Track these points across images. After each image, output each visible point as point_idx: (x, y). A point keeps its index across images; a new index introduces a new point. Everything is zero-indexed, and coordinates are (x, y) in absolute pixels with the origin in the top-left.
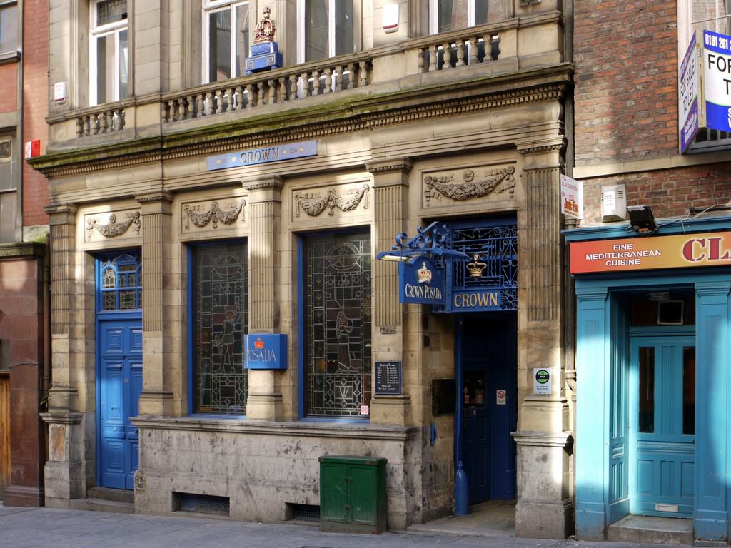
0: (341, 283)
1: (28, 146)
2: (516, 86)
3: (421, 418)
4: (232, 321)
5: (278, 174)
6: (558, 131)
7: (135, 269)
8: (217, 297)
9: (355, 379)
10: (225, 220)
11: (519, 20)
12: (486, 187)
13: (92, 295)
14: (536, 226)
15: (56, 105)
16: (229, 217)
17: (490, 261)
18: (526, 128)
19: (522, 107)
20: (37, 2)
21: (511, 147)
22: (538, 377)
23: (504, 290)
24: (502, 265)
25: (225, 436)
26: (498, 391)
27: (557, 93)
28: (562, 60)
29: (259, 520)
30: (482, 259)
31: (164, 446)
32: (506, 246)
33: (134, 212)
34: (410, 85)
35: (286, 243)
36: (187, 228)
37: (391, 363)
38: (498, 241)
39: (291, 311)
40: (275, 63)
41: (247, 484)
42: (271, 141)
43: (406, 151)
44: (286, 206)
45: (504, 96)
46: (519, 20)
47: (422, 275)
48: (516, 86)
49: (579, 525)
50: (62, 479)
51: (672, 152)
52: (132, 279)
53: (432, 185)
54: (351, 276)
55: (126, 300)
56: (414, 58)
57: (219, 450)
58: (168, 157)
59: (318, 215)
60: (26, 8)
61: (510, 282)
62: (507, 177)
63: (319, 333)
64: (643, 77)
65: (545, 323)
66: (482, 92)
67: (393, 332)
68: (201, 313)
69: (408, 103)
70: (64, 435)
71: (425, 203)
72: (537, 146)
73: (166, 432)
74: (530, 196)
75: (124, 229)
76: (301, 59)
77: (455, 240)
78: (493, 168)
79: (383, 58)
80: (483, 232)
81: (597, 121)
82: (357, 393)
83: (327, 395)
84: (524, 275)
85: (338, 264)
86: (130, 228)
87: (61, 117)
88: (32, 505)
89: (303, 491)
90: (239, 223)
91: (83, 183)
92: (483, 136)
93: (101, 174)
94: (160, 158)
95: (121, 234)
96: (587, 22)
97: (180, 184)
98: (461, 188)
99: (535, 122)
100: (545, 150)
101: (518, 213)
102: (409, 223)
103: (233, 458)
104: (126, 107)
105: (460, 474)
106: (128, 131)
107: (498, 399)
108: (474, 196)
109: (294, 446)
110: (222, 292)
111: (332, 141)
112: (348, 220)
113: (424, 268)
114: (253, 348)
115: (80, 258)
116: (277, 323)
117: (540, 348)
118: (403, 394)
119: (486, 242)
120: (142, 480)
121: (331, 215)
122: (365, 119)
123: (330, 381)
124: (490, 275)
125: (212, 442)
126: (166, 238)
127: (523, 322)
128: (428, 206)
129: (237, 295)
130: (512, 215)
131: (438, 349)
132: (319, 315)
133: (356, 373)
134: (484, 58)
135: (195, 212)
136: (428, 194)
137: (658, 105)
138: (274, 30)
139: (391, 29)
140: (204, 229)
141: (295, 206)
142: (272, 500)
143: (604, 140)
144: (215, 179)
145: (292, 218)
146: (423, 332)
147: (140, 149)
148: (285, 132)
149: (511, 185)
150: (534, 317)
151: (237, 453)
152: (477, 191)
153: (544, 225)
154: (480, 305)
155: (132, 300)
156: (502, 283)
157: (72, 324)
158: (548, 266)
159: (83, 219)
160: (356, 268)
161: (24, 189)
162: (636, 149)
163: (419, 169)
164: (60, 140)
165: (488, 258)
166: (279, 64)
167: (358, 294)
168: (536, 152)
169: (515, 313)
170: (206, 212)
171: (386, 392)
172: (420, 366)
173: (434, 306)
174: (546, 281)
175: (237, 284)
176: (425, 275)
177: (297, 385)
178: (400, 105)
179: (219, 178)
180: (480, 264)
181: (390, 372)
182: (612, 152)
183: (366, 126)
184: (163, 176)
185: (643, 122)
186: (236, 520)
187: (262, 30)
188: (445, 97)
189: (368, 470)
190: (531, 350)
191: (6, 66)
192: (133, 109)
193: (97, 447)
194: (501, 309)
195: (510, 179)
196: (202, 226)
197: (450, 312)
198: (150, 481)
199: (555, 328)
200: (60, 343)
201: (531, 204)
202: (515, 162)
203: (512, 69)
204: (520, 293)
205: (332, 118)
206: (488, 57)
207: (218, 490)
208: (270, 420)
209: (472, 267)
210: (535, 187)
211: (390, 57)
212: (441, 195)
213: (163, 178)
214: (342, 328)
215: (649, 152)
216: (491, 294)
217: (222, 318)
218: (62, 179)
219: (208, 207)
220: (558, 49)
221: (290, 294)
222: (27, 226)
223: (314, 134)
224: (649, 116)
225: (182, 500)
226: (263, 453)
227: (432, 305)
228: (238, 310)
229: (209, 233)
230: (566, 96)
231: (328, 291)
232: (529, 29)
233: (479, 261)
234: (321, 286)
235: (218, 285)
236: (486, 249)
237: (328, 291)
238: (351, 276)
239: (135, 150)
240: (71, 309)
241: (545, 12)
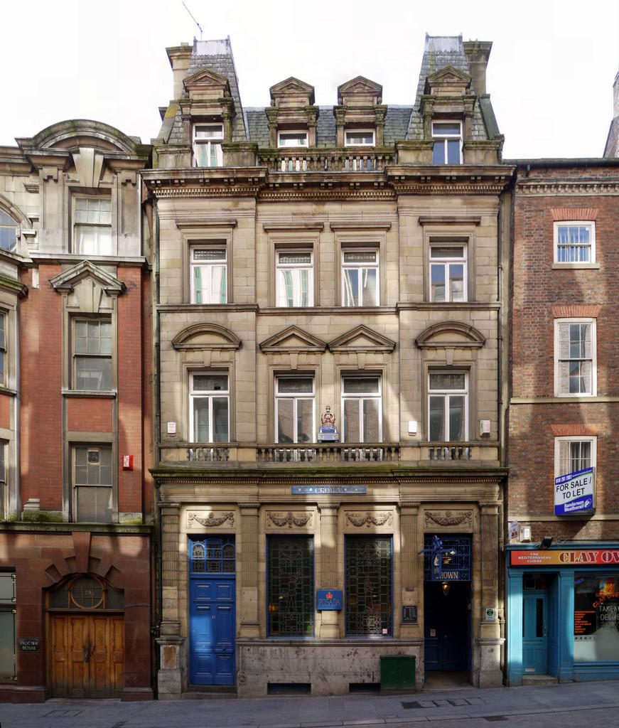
2: (483, 474)
18: (483, 494)
19: (481, 485)
22: (488, 612)
25: (306, 648)
28: (501, 466)
29: (331, 694)
31: (260, 656)
35: (341, 540)
41: (323, 675)
48: (483, 474)
49: (511, 679)
50: (175, 681)
51: (550, 514)
52: (218, 554)
57: (302, 657)
59: (360, 526)
64: (540, 480)
65: (491, 588)
66: (466, 474)
69: (426, 474)
70: (175, 652)
71: (425, 526)
73: (262, 648)
75: (221, 522)
79: (406, 449)
80: (450, 542)
81: (518, 496)
86: (225, 522)
88: (150, 699)
89: (361, 676)
90: (308, 526)
93: (207, 486)
96: (514, 450)
100: (493, 506)
103: (312, 661)
104: (231, 447)
109: (353, 652)
111: (376, 487)
112: (380, 530)
115: (183, 538)
120: (244, 677)
121: (368, 526)
125: (297, 652)
127: (477, 586)
130: (470, 536)
135: (276, 517)
137: (546, 493)
139: (412, 434)
140: (283, 527)
142: (342, 682)
143: (523, 505)
147: (246, 475)
151: (315, 658)
159: (186, 514)
160: (376, 556)
162: (536, 511)
164: (171, 460)
170: (283, 517)
171: (409, 621)
178: (421, 474)
179: (300, 499)
182: (525, 511)
185: (539, 499)
186: (316, 696)
188: (447, 474)
191: (103, 400)
193: (193, 660)
196: (280, 526)
198: (250, 678)
200: (169, 593)
205: (381, 475)
207: (302, 679)
208: (337, 638)
215: (541, 513)
217: (287, 580)
219: (285, 515)
222: (123, 512)
224: (542, 497)
225: (273, 688)
226: (333, 656)
229: (285, 530)
230: (503, 483)
239: (243, 475)
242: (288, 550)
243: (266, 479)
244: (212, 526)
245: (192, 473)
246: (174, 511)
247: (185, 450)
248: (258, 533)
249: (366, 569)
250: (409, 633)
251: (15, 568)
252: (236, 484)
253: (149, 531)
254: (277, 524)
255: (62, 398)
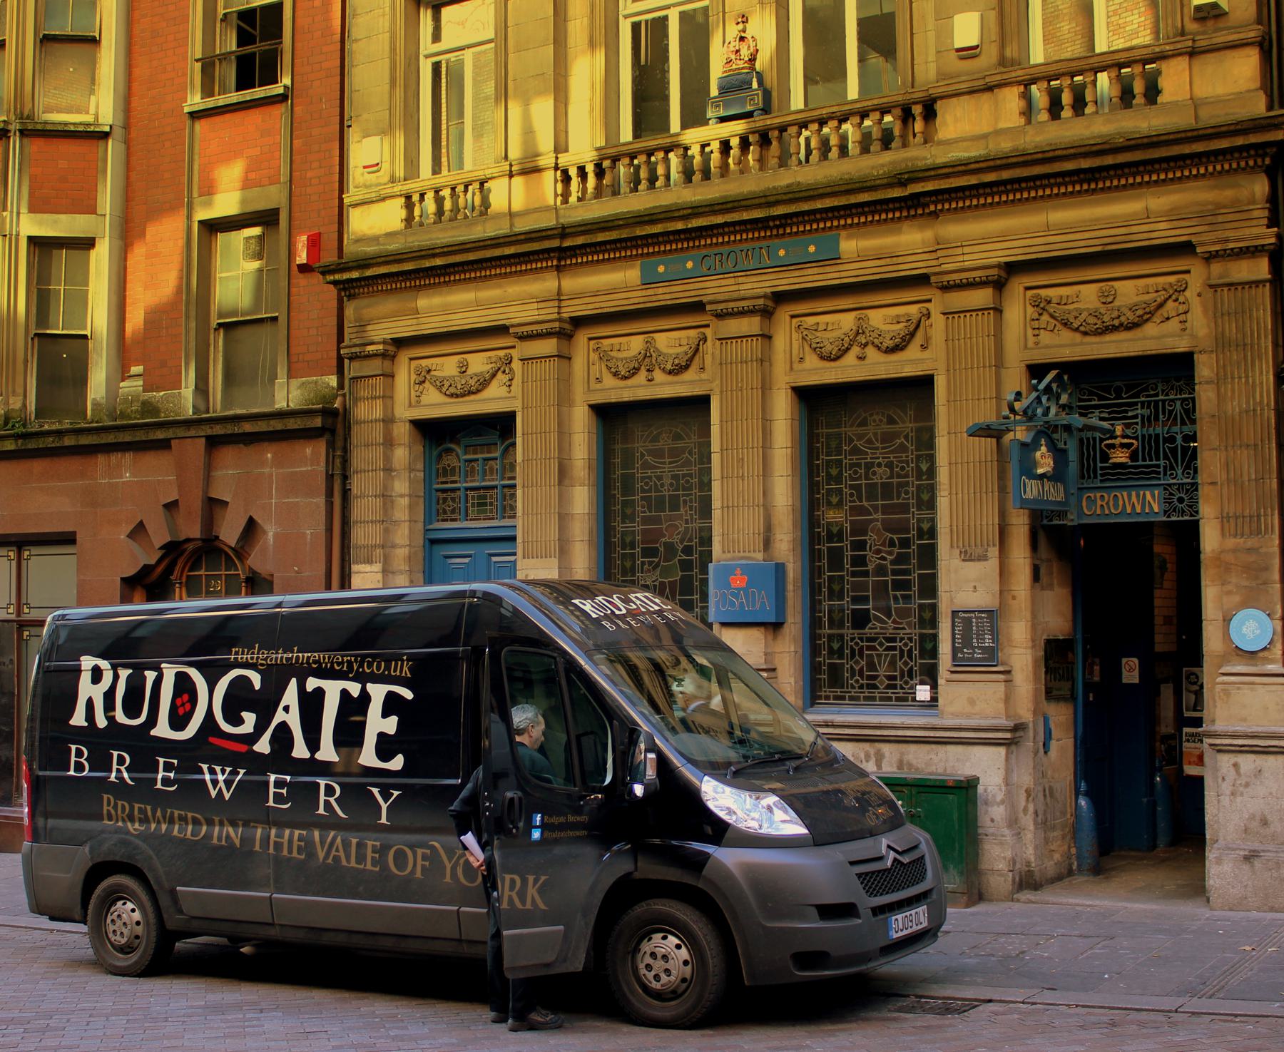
0: (874, 473)
1: (302, 242)
3: (1031, 706)
4: (676, 539)
5: (769, 290)
6: (1265, 221)
7: (496, 451)
8: (858, 488)
9: (902, 639)
10: (669, 367)
11: (1194, 41)
12: (1140, 312)
13: (419, 497)
14: (1233, 378)
15: (363, 174)
16: (677, 362)
17: (1143, 436)
19: (1200, 183)
20: (318, 3)
21: (1184, 249)
23: (1170, 485)
24: (1164, 444)
26: (1124, 660)
27: (1263, 161)
28: (1270, 107)
30: (1129, 432)
32: (1171, 412)
33: (502, 353)
34: (1005, 145)
36: (599, 380)
37: (980, 612)
38: (1156, 402)
39: (790, 523)
40: (761, 105)
42: (418, 283)
43: (1000, 253)
44: (579, 364)
45: (1172, 164)
46: (1194, 41)
47: (1042, 462)
52: (491, 469)
53: (1043, 309)
54: (892, 462)
55: (479, 505)
56: (1011, 99)
58: (568, 262)
59: (837, 358)
60: (299, 13)
61: (1180, 472)
62: (1174, 297)
63: (836, 559)
65: (1251, 542)
67: (982, 558)
68: (620, 527)
69: (1006, 175)
71: (1031, 340)
72: (1231, 245)
74: (1220, 329)
75: (484, 384)
76: (797, 102)
77: (1080, 400)
78: (1161, 280)
82: (906, 664)
83: (852, 667)
84: (1211, 462)
85: (870, 441)
86: (495, 383)
87: (373, 195)
91: (414, 305)
92: (1134, 229)
94: (555, 263)
95: (478, 391)
97: (591, 306)
98: (1095, 314)
99: (1225, 207)
101: (1195, 356)
102: (1003, 371)
105: (1083, 802)
106: (499, 216)
107: (1125, 673)
108: (1117, 327)
110: (657, 490)
113: (1044, 449)
114: (728, 586)
116: (767, 543)
117: (1246, 583)
118: (1002, 664)
119: (1136, 404)
121: (861, 358)
122: (928, 199)
123: (857, 644)
124: (1144, 460)
126: (564, 400)
127: (1210, 539)
128: (1037, 343)
129: (683, 495)
131: (1050, 587)
132: (835, 530)
133: (904, 628)
134: (1134, 102)
135: (613, 354)
136: (1036, 324)
138: (757, 51)
140: (629, 382)
141: (795, 345)
144: (654, 298)
145: (791, 363)
146: (1032, 558)
148: (783, 221)
149: (1182, 309)
150: (1232, 532)
152: (1123, 319)
153: (1247, 377)
154: (1129, 510)
155: (491, 504)
156: (1165, 474)
157: (387, 546)
158: (1256, 445)
161: (292, 314)
163: (1017, 286)
165: (1139, 432)
166: (766, 110)
167: (907, 493)
168: (1229, 255)
169: (1195, 525)
170: (633, 352)
171: (972, 662)
172: (1029, 616)
173: (1045, 513)
174: (1252, 471)
175: (684, 476)
176: (1044, 461)
177: (800, 651)
180: (1126, 441)
181: (977, 627)
183: (927, 211)
184: (559, 292)
187: (738, 51)
189: (951, 797)
190: (1230, 587)
192: (1182, 63)
194: (1165, 519)
195: (507, 372)
196: (626, 378)
197: (1075, 523)
199: (1271, 550)
201: (1221, 343)
202: (1188, 272)
203: (1183, 120)
204: (1204, 491)
206: (1139, 100)
209: (1112, 446)
210: (1229, 314)
211: (966, 97)
212: (1059, 326)
213: (559, 297)
214: (878, 552)
216: (1148, 493)
218: (373, 300)
220: (1261, 88)
221: (790, 494)
223: (744, 236)
227: (1042, 511)
228: (687, 522)
231: (852, 487)
232: (1209, 56)
233: (1124, 437)
234: (838, 479)
235: (650, 478)
236: (1135, 417)
237: (852, 487)
238: (892, 462)
240: (386, 521)
241: (1236, 28)
242: (660, 445)
243: (574, 251)
244: (463, 395)
245: (367, 266)
246: (375, 366)
247: (1016, 91)
248: (766, 388)
249: (872, 492)
250: (972, 702)
251: (74, 533)
252: (446, 283)
253: (318, 422)
254: (616, 374)
255: (188, 122)
